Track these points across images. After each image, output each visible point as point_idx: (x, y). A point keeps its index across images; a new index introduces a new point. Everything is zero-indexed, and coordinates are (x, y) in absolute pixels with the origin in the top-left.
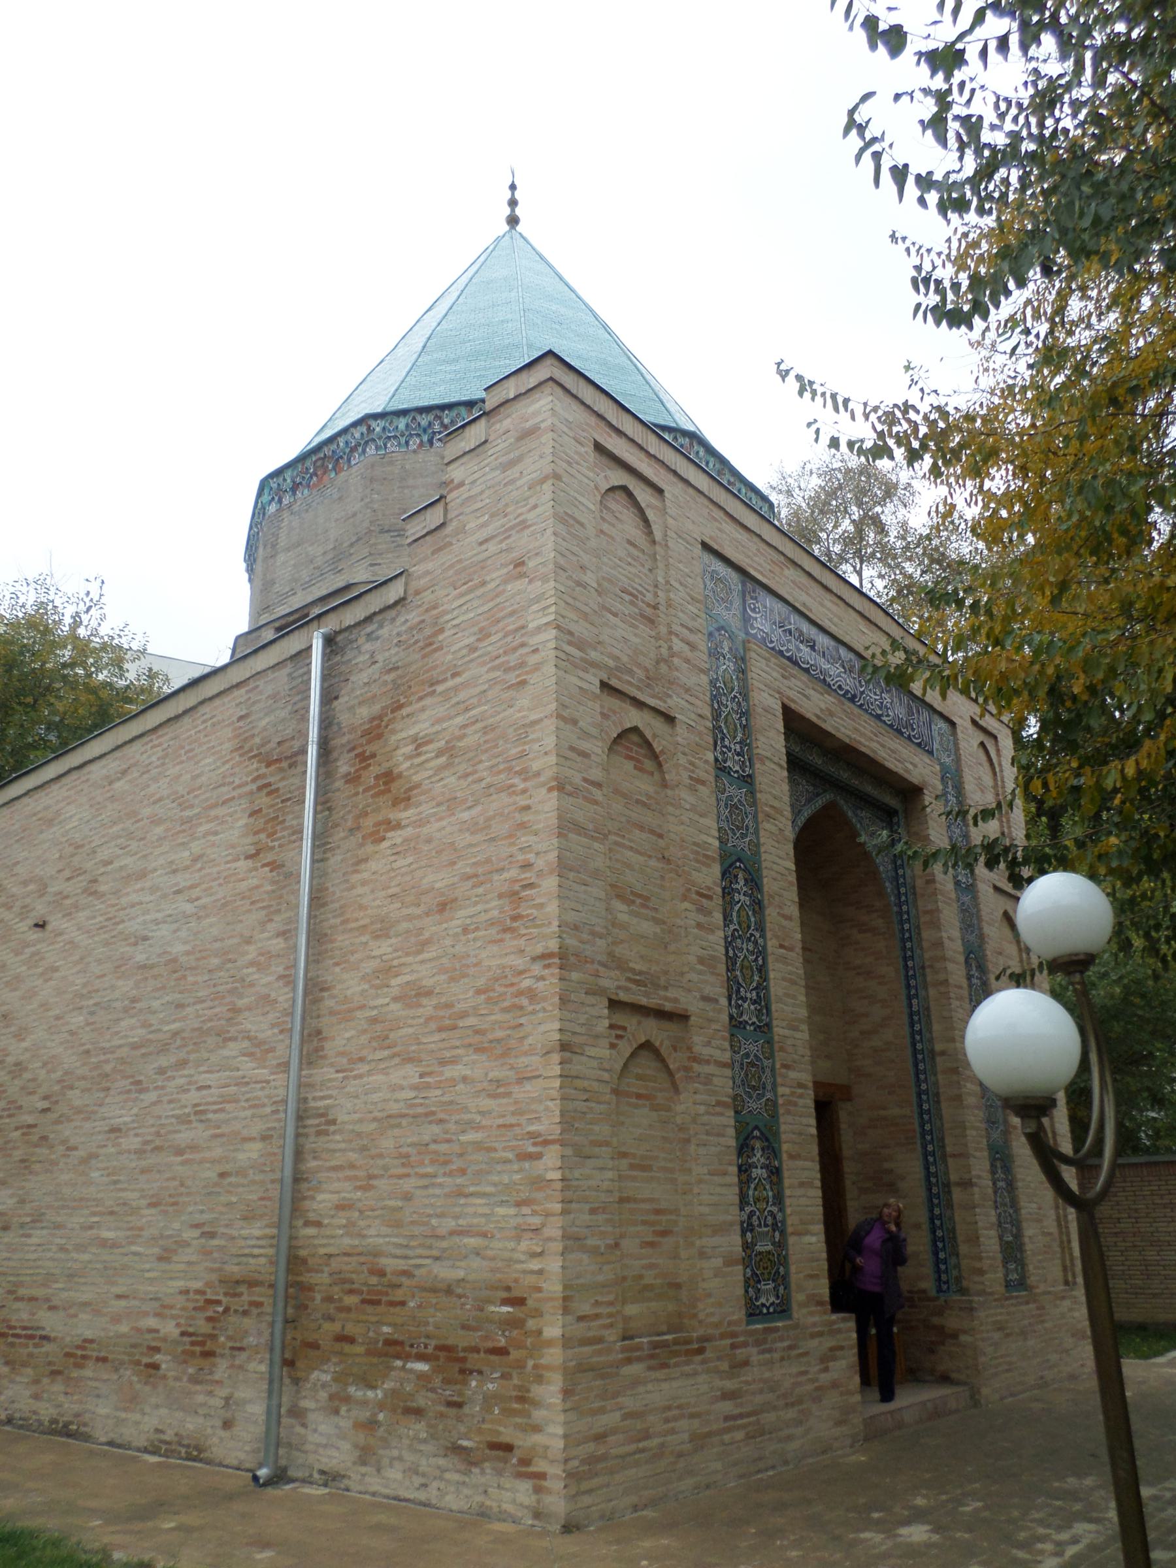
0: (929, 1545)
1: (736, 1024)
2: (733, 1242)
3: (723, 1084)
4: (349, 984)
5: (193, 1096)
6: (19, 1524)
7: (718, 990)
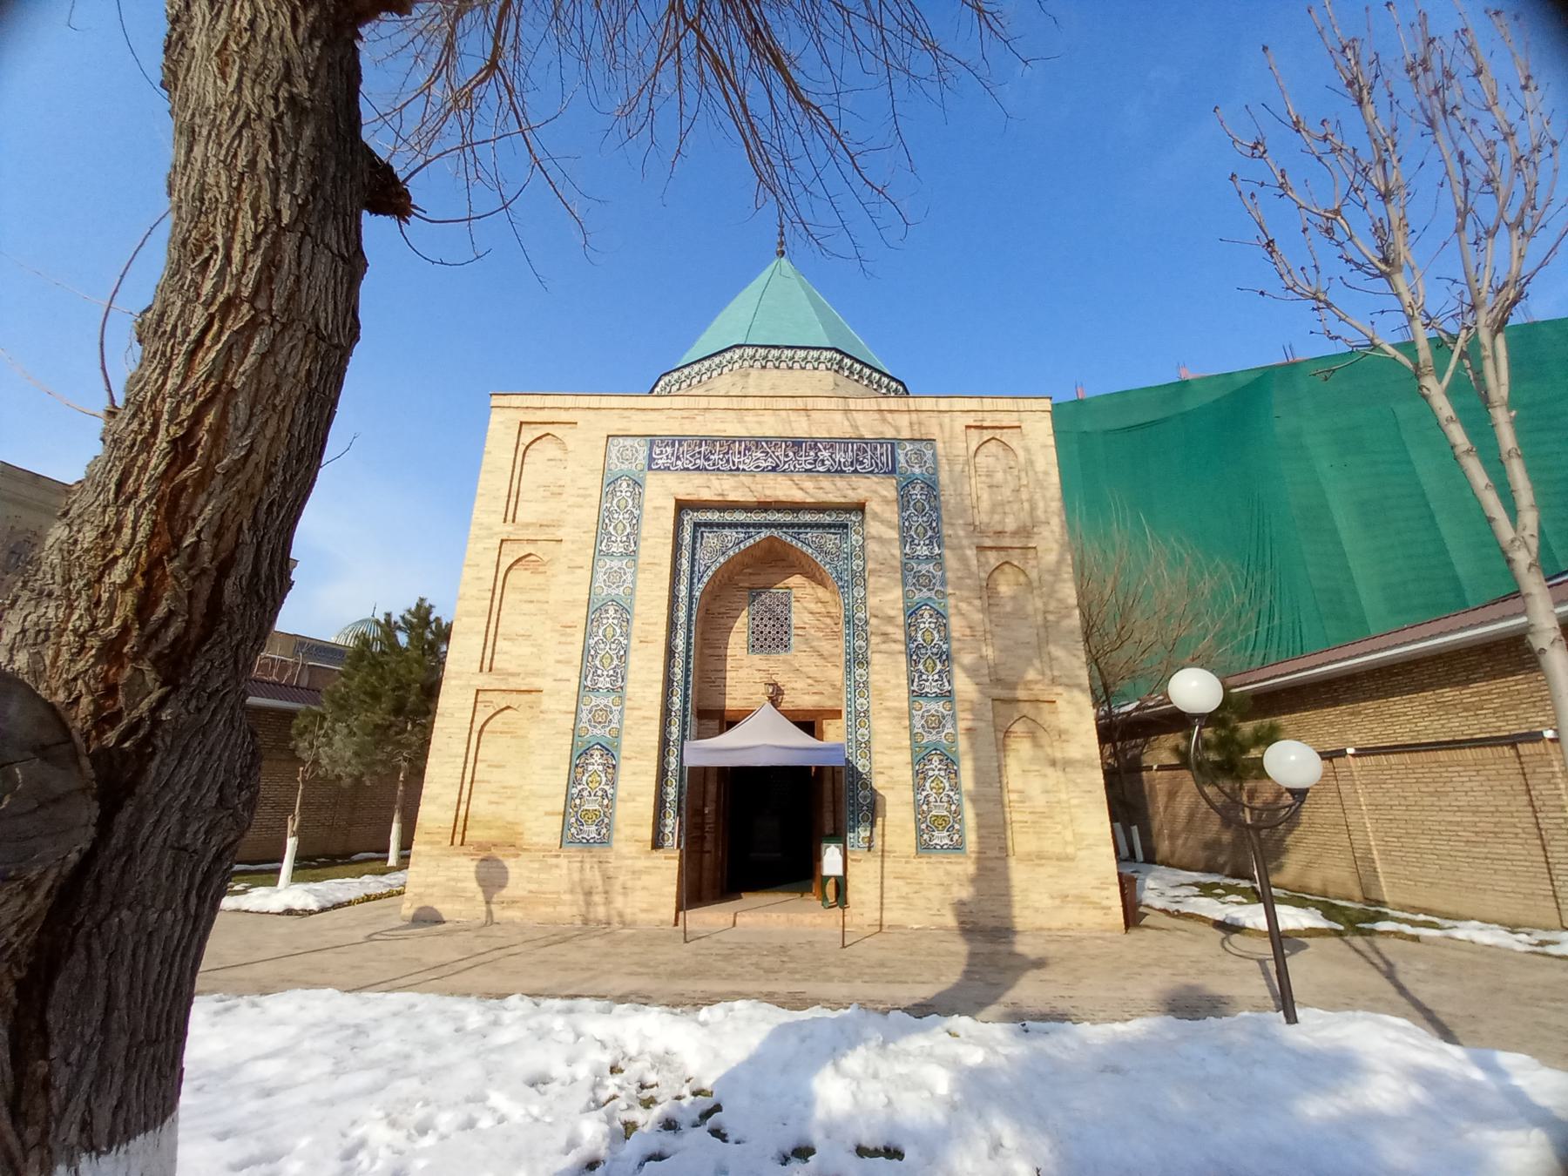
1: (584, 690)
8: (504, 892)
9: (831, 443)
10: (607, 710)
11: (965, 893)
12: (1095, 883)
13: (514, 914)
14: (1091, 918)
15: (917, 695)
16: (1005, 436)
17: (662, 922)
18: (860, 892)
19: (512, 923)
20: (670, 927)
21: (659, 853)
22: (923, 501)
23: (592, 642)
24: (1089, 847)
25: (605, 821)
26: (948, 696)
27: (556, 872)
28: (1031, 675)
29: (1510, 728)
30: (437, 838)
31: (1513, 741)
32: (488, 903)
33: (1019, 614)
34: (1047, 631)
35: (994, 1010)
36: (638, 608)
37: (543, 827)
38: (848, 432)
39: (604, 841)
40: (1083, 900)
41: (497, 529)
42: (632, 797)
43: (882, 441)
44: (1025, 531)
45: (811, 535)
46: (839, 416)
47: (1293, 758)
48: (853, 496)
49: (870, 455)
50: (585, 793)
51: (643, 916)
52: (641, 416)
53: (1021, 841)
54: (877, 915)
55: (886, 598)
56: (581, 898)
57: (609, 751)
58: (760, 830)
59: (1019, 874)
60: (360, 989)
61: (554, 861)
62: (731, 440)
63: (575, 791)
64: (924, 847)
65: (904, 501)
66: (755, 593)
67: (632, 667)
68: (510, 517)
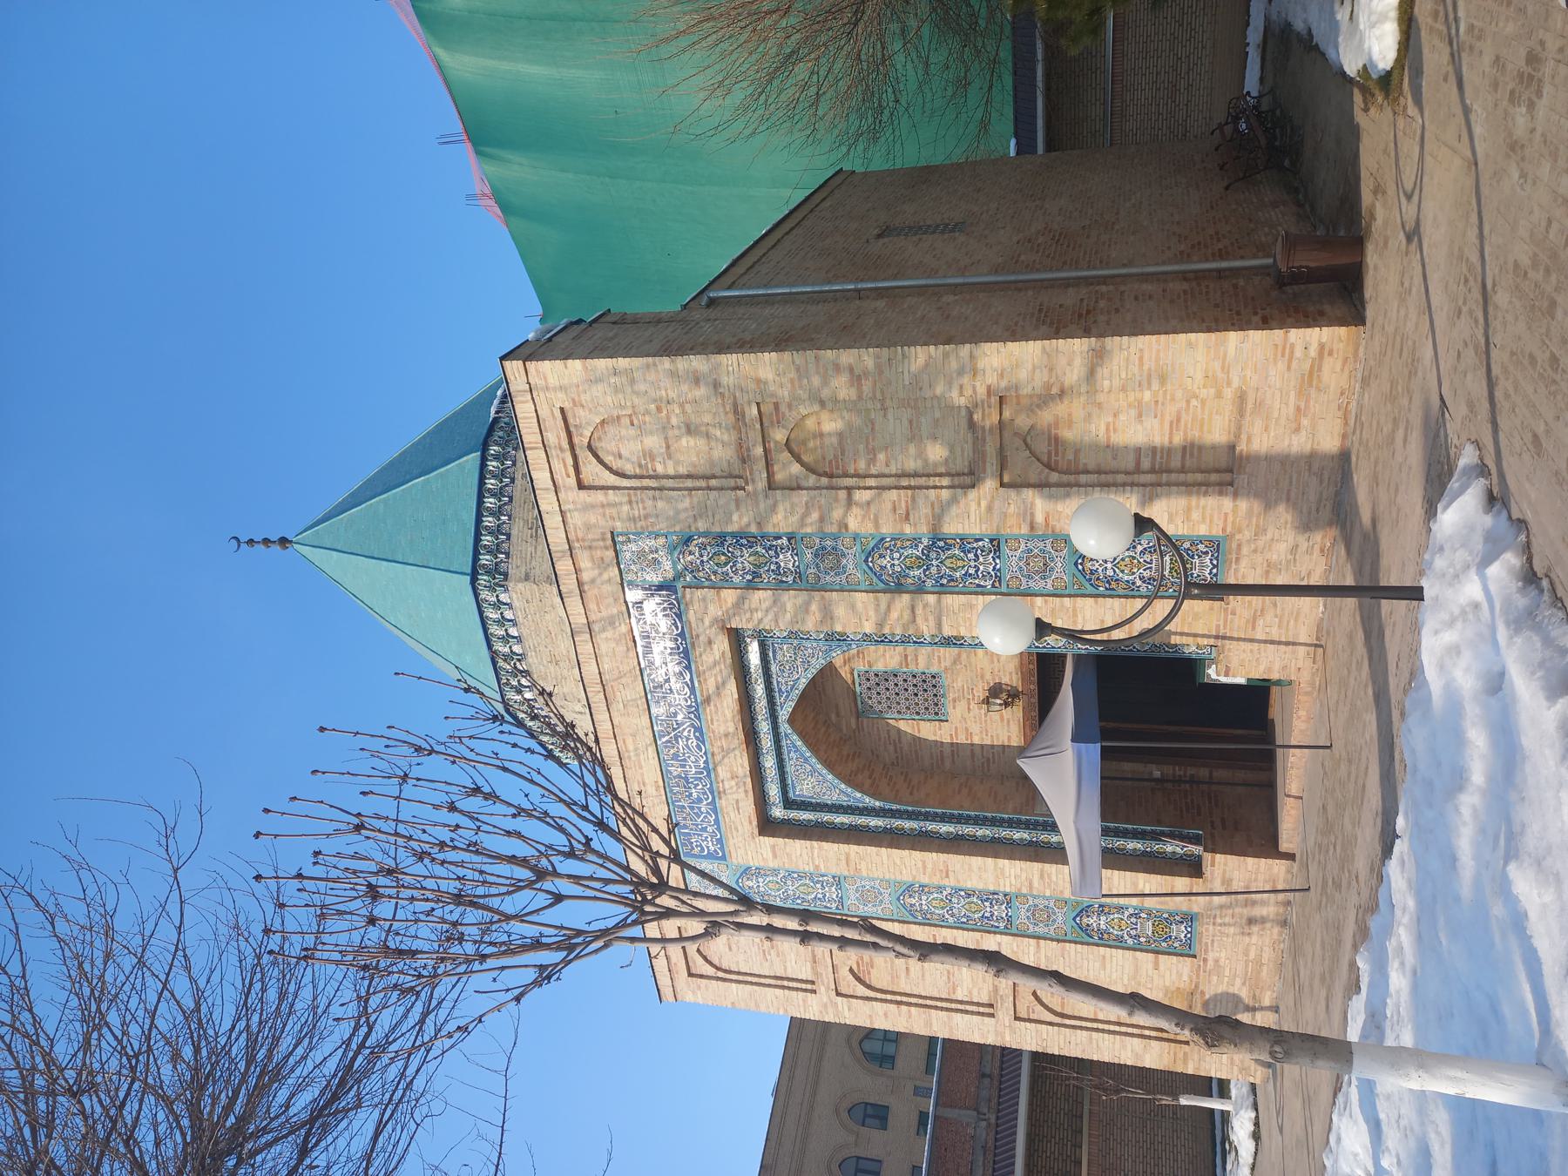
12: (1281, 366)
14: (1334, 375)
17: (1288, 871)
18: (1270, 670)
20: (1296, 866)
21: (1207, 869)
23: (951, 920)
24: (1226, 369)
30: (1181, 1055)
35: (1454, 484)
36: (907, 877)
40: (1311, 378)
41: (825, 999)
47: (1092, 542)
50: (1133, 933)
54: (1302, 650)
56: (1255, 929)
58: (1178, 747)
60: (1345, 1018)
61: (1210, 963)
63: (1130, 942)
64: (1187, 950)
66: (861, 712)
67: (981, 886)
68: (809, 987)
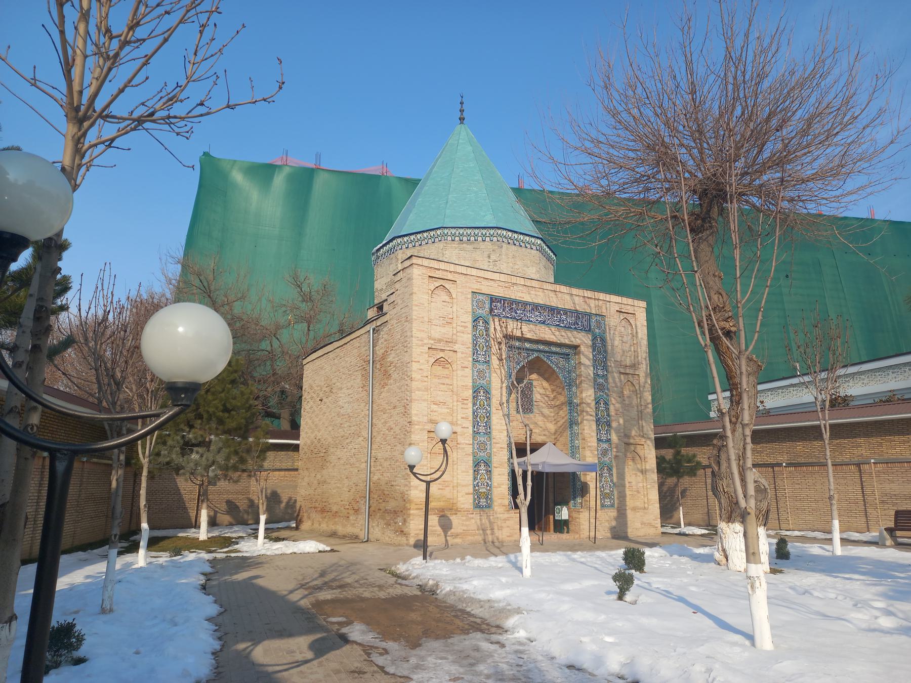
0: (208, 507)
1: (476, 433)
2: (471, 489)
3: (470, 449)
4: (379, 424)
5: (353, 450)
6: (465, 586)
7: (469, 424)
8: (452, 530)
9: (566, 312)
10: (484, 444)
11: (614, 523)
13: (458, 541)
15: (599, 440)
16: (629, 317)
19: (457, 544)
22: (600, 346)
25: (488, 496)
26: (609, 440)
27: (473, 521)
28: (633, 433)
29: (771, 461)
31: (772, 466)
32: (446, 536)
33: (630, 405)
34: (641, 415)
37: (465, 500)
38: (569, 306)
39: (489, 506)
40: (650, 525)
42: (499, 486)
43: (586, 314)
44: (634, 366)
45: (554, 358)
46: (568, 297)
48: (576, 342)
49: (581, 320)
51: (509, 539)
52: (485, 282)
53: (630, 503)
55: (588, 394)
57: (487, 464)
59: (630, 514)
62: (526, 304)
65: (594, 347)
